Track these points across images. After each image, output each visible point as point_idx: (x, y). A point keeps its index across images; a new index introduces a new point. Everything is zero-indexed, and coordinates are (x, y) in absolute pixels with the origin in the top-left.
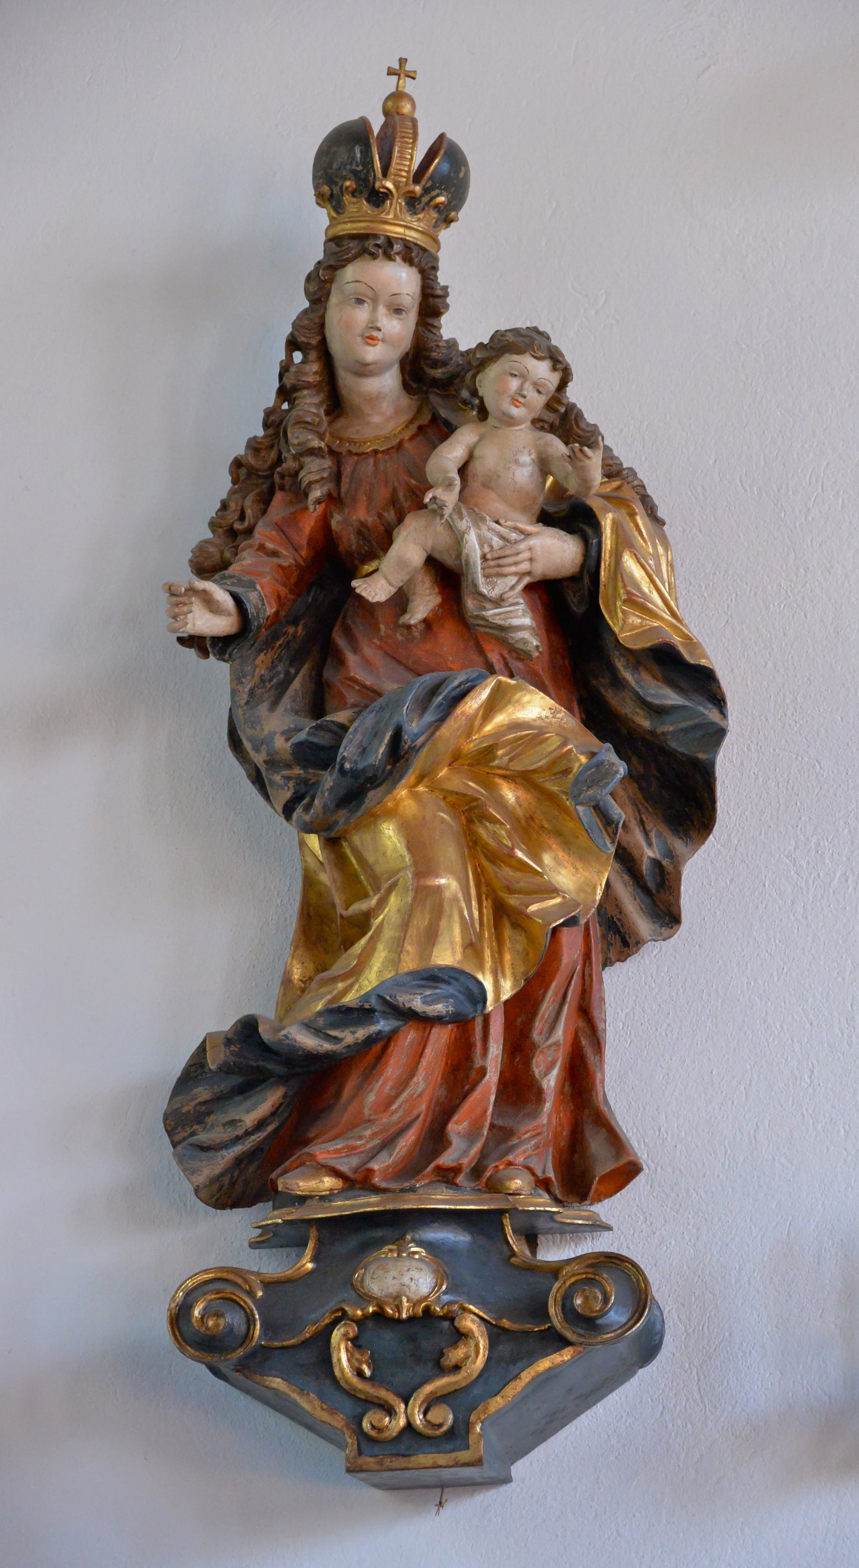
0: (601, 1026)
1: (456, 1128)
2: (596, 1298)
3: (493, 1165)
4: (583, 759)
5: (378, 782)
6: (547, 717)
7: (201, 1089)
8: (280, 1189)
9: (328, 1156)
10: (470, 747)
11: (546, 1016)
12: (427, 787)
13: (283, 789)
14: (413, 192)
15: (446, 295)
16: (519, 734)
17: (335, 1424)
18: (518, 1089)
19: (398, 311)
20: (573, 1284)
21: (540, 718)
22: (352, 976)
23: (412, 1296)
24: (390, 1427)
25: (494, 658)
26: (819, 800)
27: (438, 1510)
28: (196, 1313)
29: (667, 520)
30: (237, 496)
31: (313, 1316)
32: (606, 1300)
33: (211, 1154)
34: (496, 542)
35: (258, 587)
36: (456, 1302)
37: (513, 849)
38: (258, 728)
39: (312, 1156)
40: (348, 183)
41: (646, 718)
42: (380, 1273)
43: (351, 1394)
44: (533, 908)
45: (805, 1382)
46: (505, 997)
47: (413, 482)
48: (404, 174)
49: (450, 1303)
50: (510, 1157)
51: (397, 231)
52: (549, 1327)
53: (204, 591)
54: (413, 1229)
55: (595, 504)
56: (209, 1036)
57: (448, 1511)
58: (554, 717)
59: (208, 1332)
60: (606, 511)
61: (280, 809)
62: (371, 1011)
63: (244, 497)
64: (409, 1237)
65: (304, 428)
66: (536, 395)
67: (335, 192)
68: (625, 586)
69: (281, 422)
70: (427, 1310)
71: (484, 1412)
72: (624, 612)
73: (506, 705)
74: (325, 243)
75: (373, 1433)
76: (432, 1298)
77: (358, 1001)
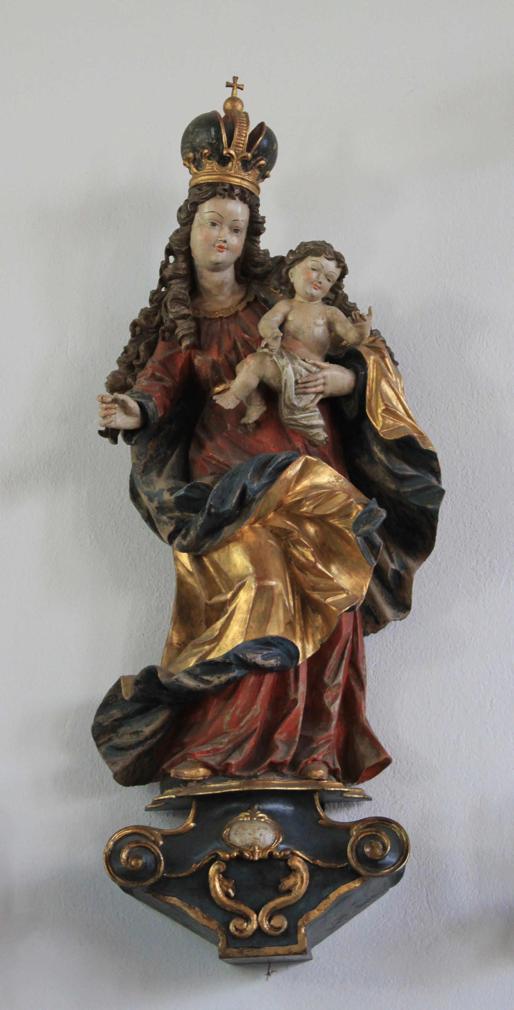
1: (280, 737)
2: (378, 847)
3: (304, 761)
4: (360, 508)
6: (333, 482)
7: (114, 711)
8: (172, 776)
9: (202, 755)
10: (289, 500)
12: (260, 524)
13: (167, 525)
14: (246, 157)
15: (264, 222)
16: (319, 492)
17: (212, 927)
18: (315, 713)
19: (236, 231)
20: (362, 839)
21: (329, 482)
22: (215, 642)
24: (247, 929)
25: (299, 445)
26: (490, 535)
27: (268, 978)
28: (124, 856)
29: (399, 362)
30: (134, 344)
31: (196, 858)
32: (385, 849)
34: (304, 372)
35: (154, 399)
37: (315, 563)
38: (152, 487)
39: (193, 755)
40: (206, 151)
42: (240, 830)
43: (221, 908)
44: (329, 600)
45: (494, 897)
46: (309, 655)
47: (247, 336)
48: (241, 145)
49: (285, 850)
50: (315, 756)
51: (236, 181)
52: (347, 865)
53: (123, 401)
54: (260, 803)
55: (363, 350)
56: (123, 678)
57: (273, 976)
58: (337, 482)
59: (131, 868)
60: (369, 354)
61: (165, 537)
62: (230, 664)
63: (139, 345)
64: (256, 807)
65: (177, 302)
66: (326, 282)
67: (197, 157)
68: (383, 401)
69: (162, 299)
71: (307, 920)
72: (383, 417)
73: (309, 474)
74: (190, 189)
75: (237, 933)
76: (274, 846)
77: (222, 658)
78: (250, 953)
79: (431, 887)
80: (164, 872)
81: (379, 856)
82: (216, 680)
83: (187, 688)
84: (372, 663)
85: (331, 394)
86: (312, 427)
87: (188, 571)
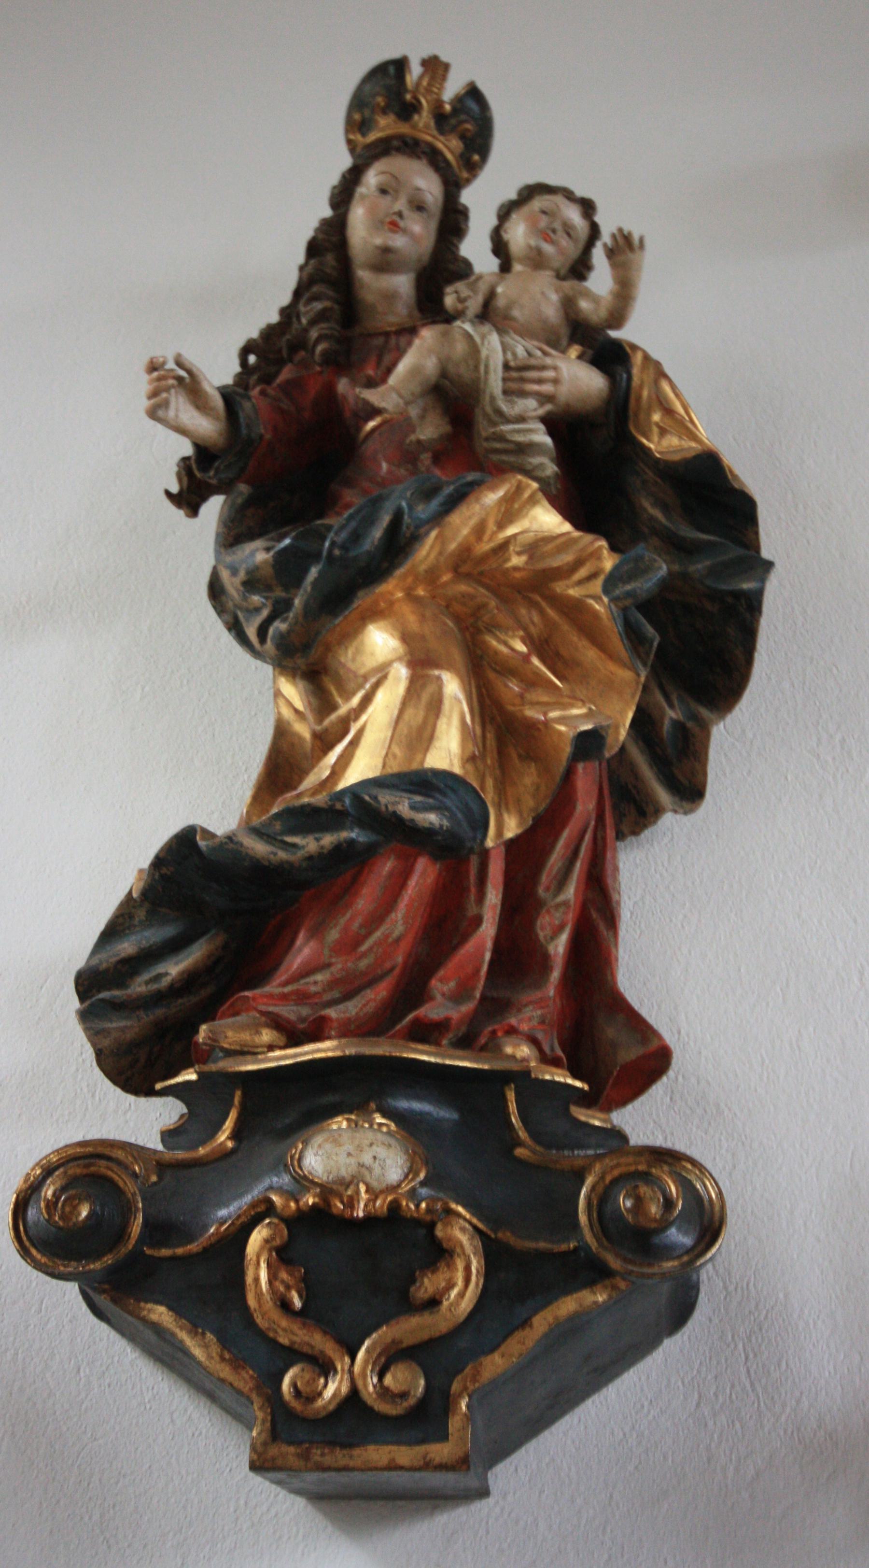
0: (615, 897)
1: (441, 985)
3: (490, 1029)
11: (554, 872)
23: (374, 1184)
36: (439, 1199)
52: (576, 1249)
75: (296, 1405)
76: (405, 1188)
78: (328, 1460)
79: (754, 1340)
80: (141, 1240)
81: (655, 1220)
82: (309, 844)
84: (629, 898)
85: (568, 405)
87: (296, 711)
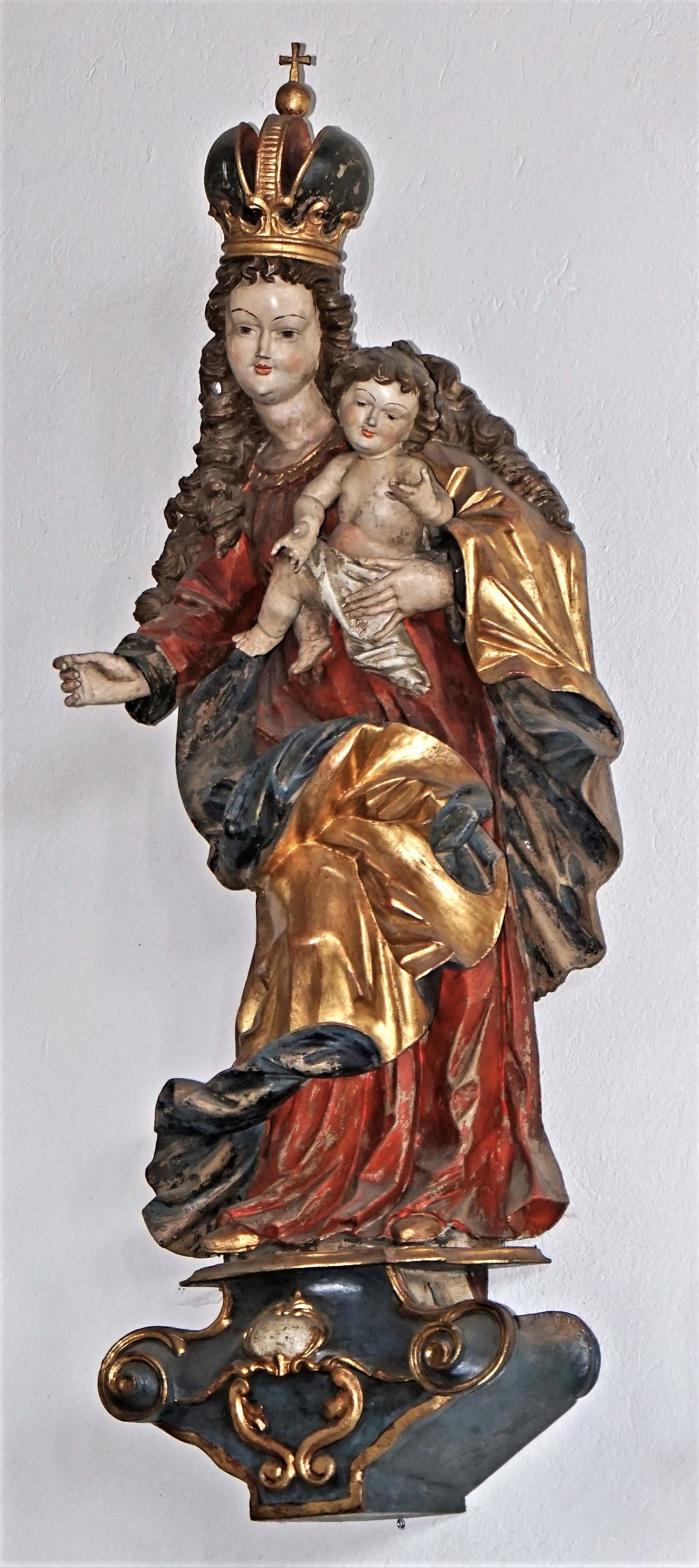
5: (266, 842)
23: (288, 1354)
33: (174, 1209)
34: (353, 585)
35: (158, 648)
41: (535, 745)
43: (250, 1445)
60: (466, 536)
70: (303, 1366)
83: (207, 1115)
86: (394, 669)
